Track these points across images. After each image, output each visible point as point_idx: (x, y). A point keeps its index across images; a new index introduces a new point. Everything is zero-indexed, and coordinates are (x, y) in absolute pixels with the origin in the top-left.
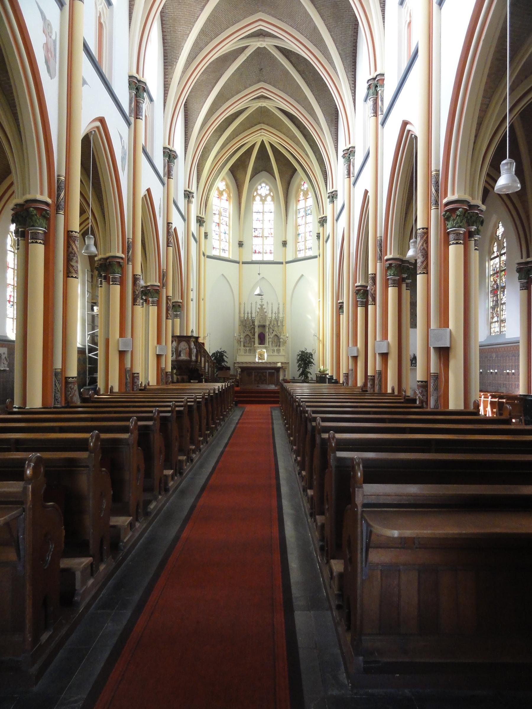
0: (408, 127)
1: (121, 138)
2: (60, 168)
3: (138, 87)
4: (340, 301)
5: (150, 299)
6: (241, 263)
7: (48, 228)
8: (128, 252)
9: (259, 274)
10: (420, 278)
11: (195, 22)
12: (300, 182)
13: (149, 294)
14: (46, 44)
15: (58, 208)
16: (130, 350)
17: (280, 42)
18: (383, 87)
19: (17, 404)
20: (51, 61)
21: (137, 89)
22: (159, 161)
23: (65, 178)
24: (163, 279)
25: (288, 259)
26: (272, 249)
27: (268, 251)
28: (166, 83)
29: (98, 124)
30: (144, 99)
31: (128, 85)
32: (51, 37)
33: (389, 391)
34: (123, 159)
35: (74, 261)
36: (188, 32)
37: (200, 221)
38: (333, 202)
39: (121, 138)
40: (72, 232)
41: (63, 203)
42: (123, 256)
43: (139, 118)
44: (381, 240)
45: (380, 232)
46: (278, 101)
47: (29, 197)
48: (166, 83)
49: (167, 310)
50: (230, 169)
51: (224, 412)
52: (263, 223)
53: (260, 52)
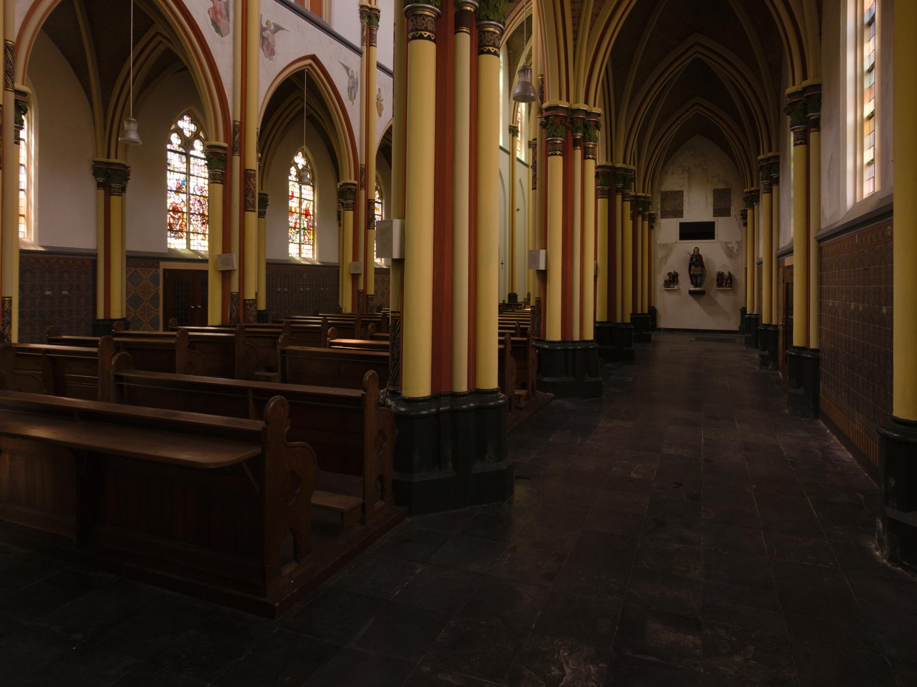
7: (225, 169)
14: (214, 8)
15: (233, 150)
21: (369, 17)
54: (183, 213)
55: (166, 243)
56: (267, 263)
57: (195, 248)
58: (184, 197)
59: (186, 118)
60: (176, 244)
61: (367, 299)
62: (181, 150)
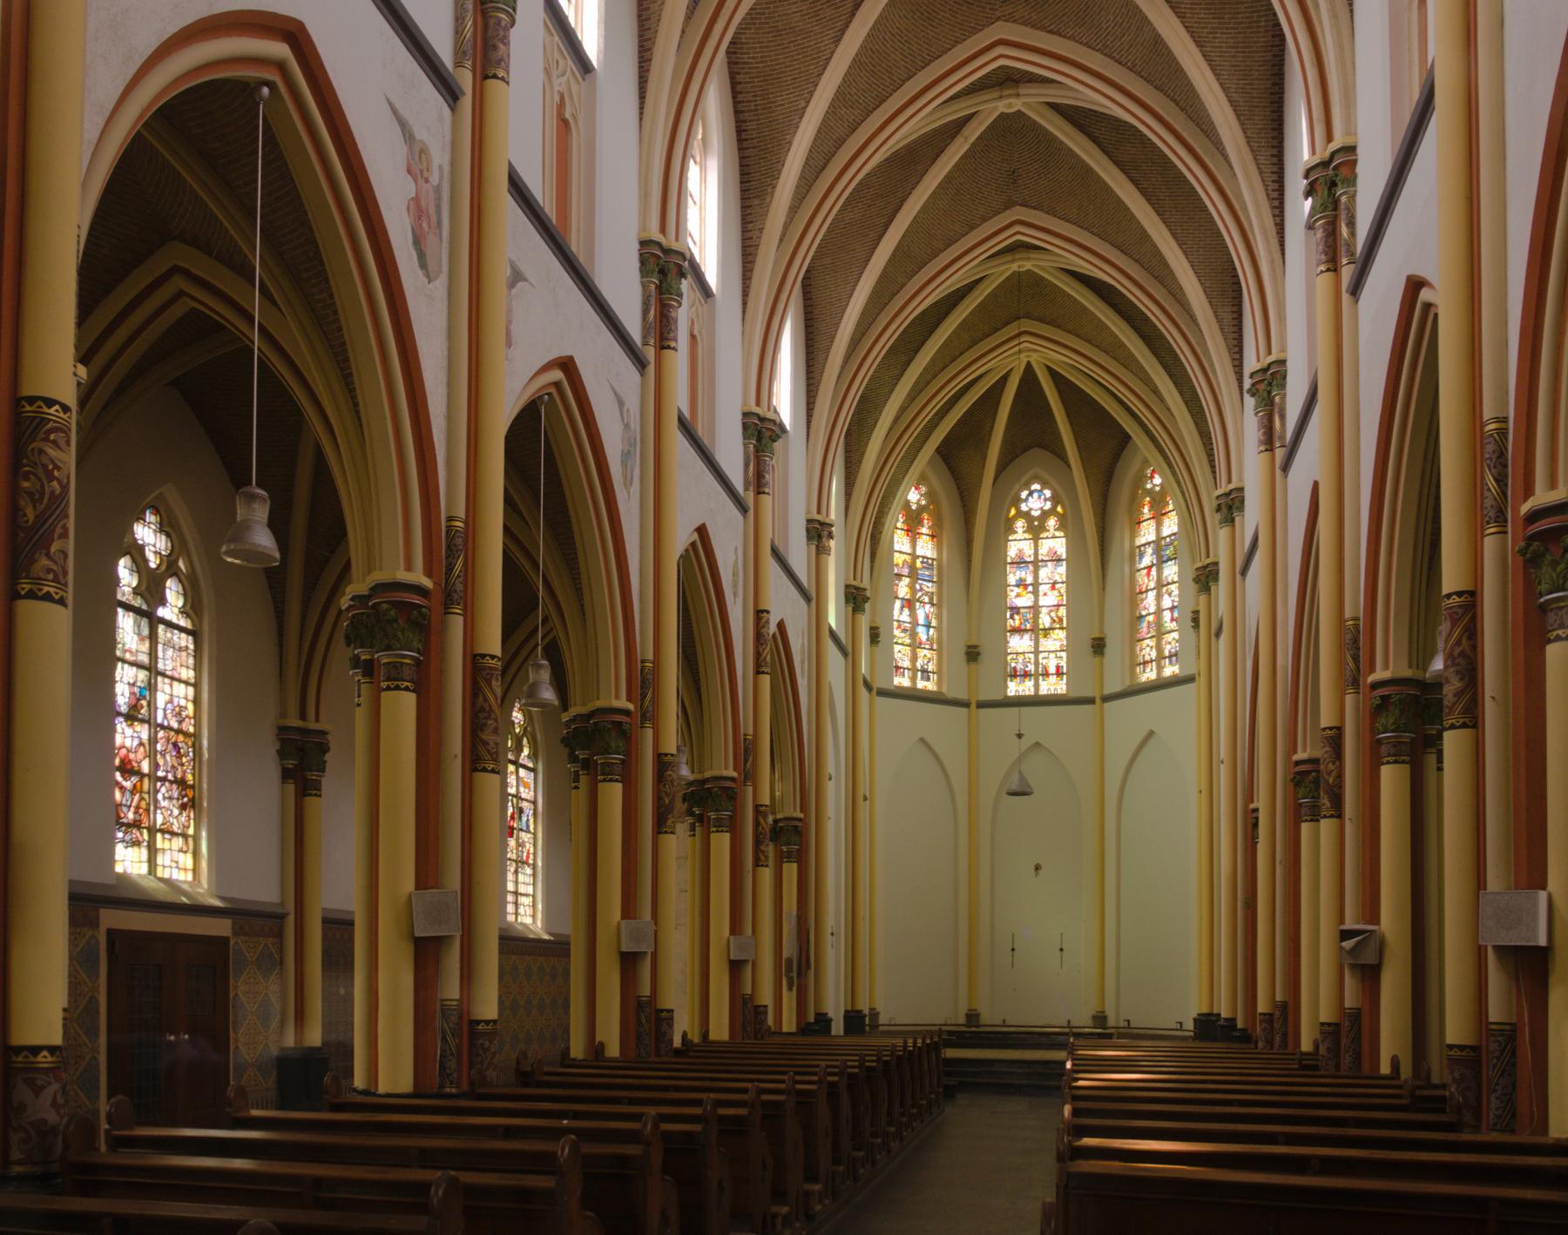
0: (1425, 295)
1: (621, 403)
2: (452, 503)
3: (665, 266)
4: (1252, 806)
5: (713, 815)
6: (974, 705)
7: (425, 651)
8: (644, 696)
9: (1020, 736)
10: (1453, 742)
11: (820, 75)
12: (1142, 470)
13: (709, 803)
14: (417, 199)
15: (448, 601)
16: (650, 950)
17: (1052, 92)
18: (1354, 185)
19: (359, 1081)
20: (430, 241)
21: (663, 272)
22: (731, 452)
23: (466, 522)
24: (746, 761)
25: (1108, 691)
26: (1063, 663)
27: (1052, 670)
28: (748, 243)
29: (557, 375)
30: (681, 295)
31: (637, 265)
32: (427, 181)
33: (1385, 1069)
34: (626, 456)
35: (489, 730)
36: (803, 104)
37: (855, 598)
38: (1233, 520)
39: (621, 403)
40: (483, 656)
41: (459, 587)
42: (631, 707)
43: (669, 347)
44: (1357, 627)
45: (1354, 605)
46: (1064, 252)
47: (380, 576)
48: (748, 243)
49: (757, 843)
50: (938, 450)
51: (902, 1115)
52: (1036, 593)
53: (1010, 128)
54: (142, 775)
55: (112, 861)
56: (325, 921)
57: (166, 876)
58: (144, 732)
59: (150, 517)
60: (129, 861)
61: (659, 1021)
62: (138, 602)
